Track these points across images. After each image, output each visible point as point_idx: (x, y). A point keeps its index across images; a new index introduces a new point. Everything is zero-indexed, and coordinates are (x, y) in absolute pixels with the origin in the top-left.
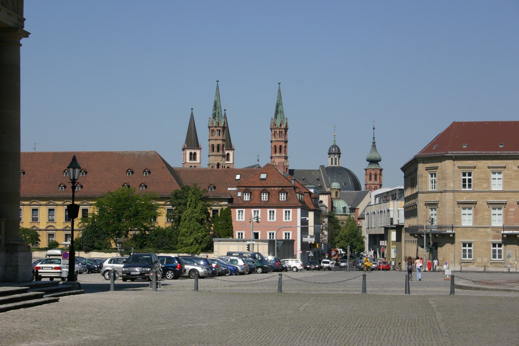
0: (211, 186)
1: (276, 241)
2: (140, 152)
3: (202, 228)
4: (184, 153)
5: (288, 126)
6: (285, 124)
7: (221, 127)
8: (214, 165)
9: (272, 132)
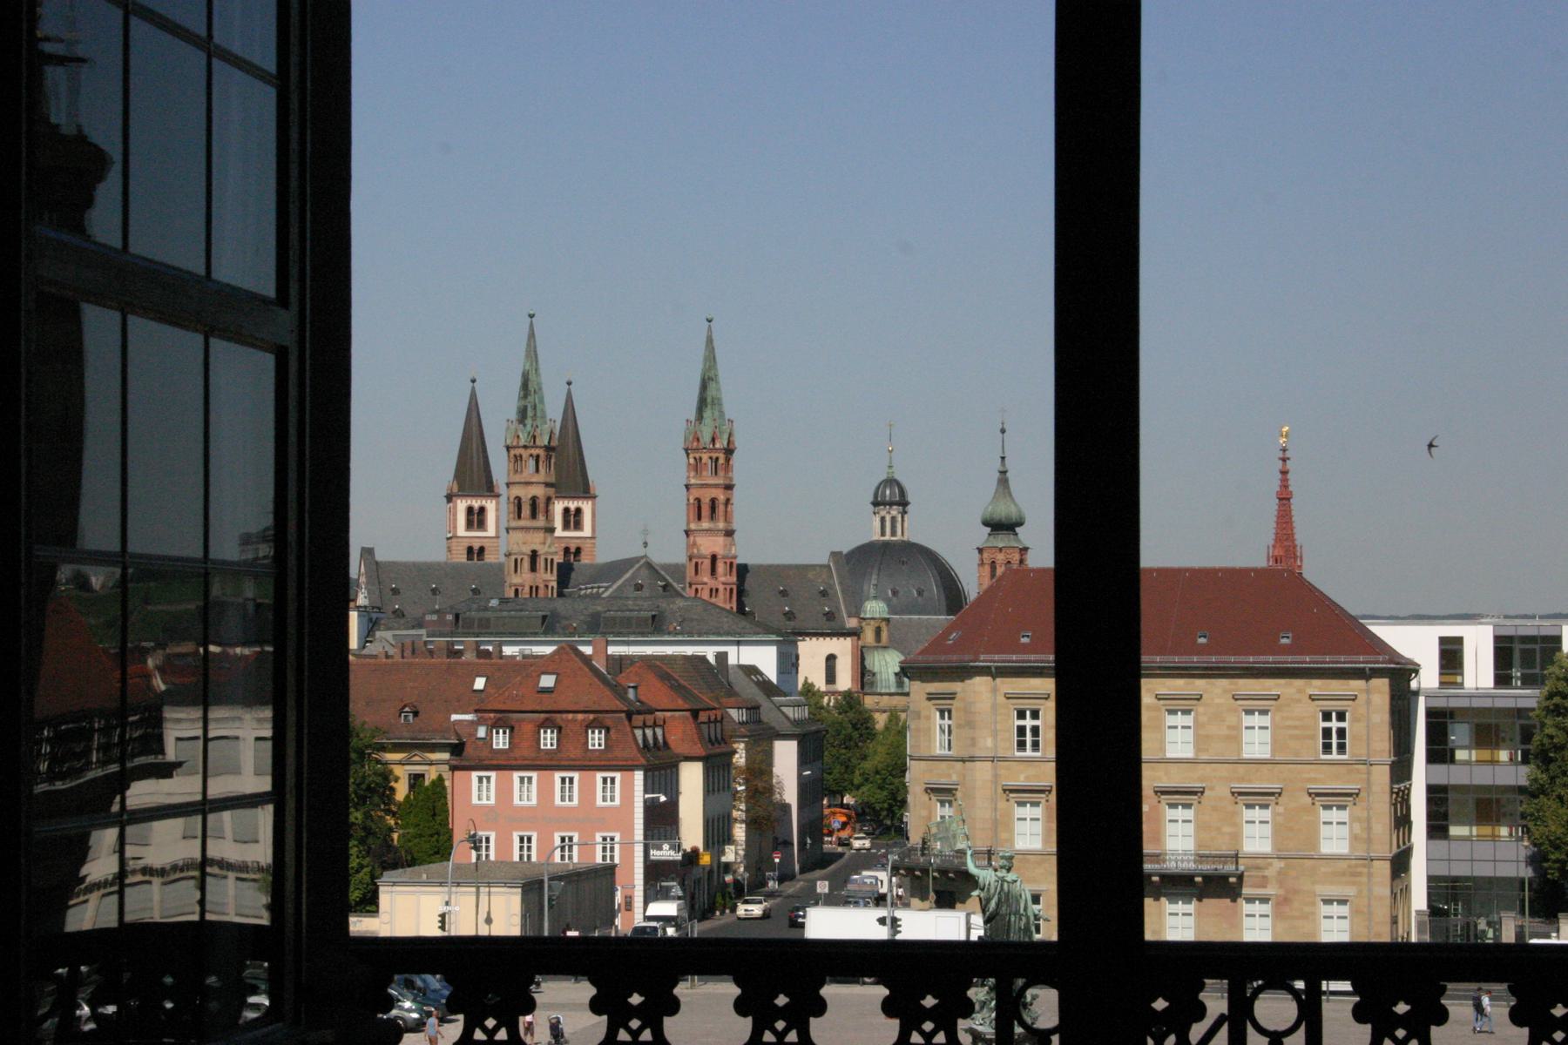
4: (450, 508)
5: (733, 444)
6: (726, 437)
7: (541, 447)
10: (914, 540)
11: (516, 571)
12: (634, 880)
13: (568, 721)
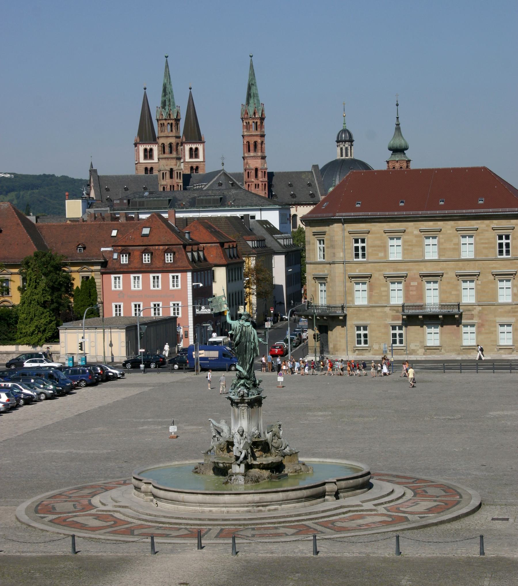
0: (80, 246)
3: (46, 312)
4: (182, 149)
6: (260, 112)
7: (173, 119)
8: (165, 172)
10: (357, 158)
11: (163, 178)
12: (188, 323)
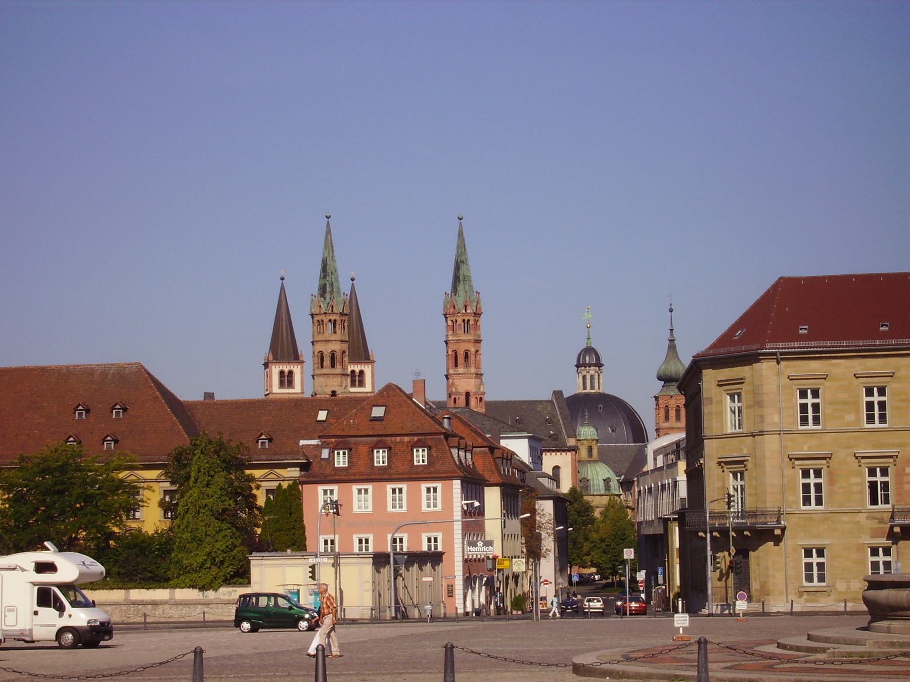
1: (392, 555)
2: (104, 365)
4: (267, 373)
6: (475, 304)
9: (446, 322)
10: (607, 392)
13: (396, 442)
